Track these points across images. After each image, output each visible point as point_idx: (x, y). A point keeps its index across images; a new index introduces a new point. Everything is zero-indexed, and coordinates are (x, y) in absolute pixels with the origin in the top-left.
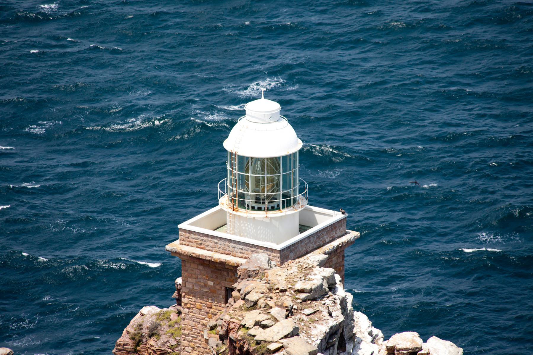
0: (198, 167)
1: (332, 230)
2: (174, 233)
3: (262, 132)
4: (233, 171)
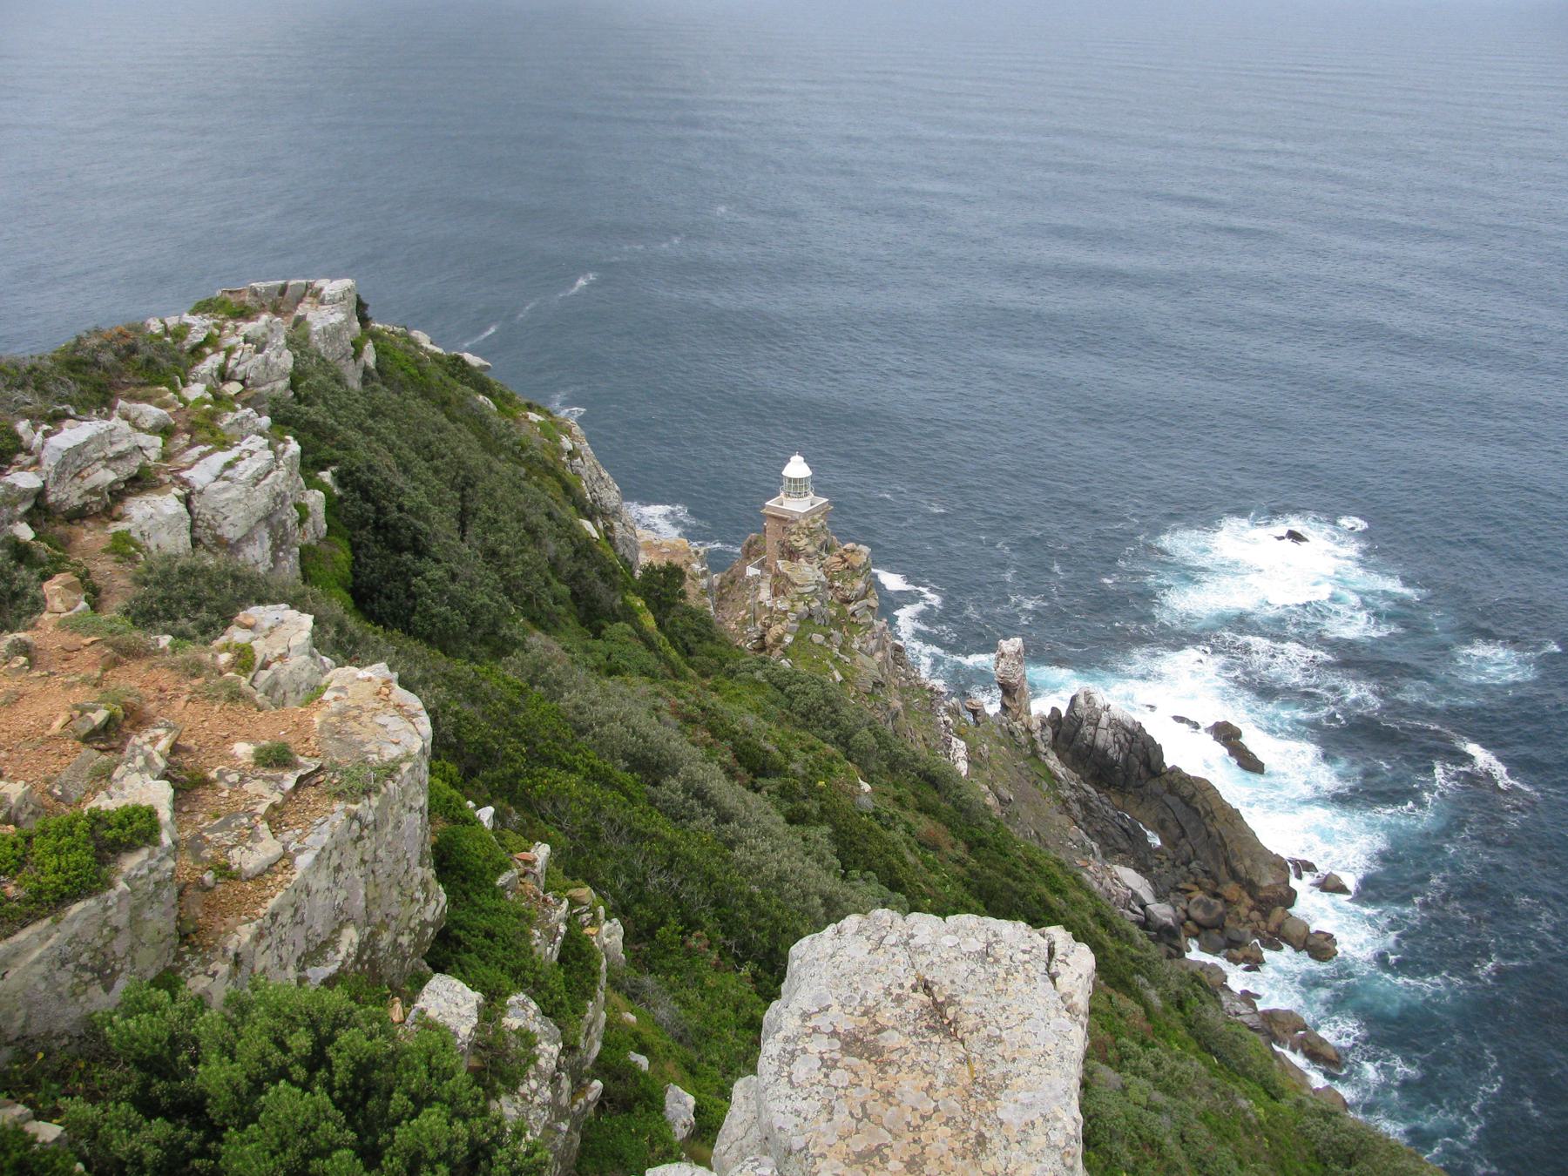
0: (774, 484)
3: (797, 468)
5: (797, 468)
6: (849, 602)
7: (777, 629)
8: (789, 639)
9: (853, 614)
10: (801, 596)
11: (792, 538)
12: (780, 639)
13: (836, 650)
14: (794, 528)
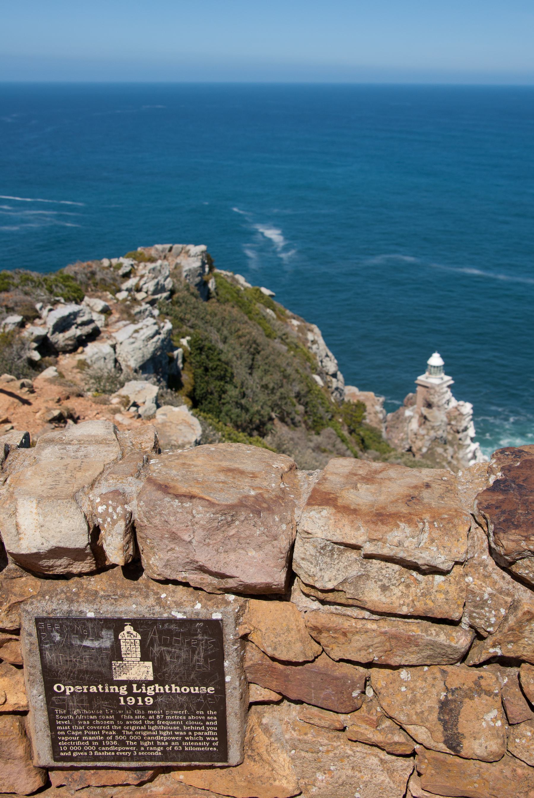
0: (423, 368)
1: (448, 381)
2: (416, 379)
3: (436, 360)
4: (429, 367)
5: (436, 360)
6: (458, 432)
7: (419, 444)
8: (424, 450)
9: (460, 439)
10: (433, 428)
11: (431, 397)
12: (420, 449)
13: (449, 458)
14: (432, 391)
